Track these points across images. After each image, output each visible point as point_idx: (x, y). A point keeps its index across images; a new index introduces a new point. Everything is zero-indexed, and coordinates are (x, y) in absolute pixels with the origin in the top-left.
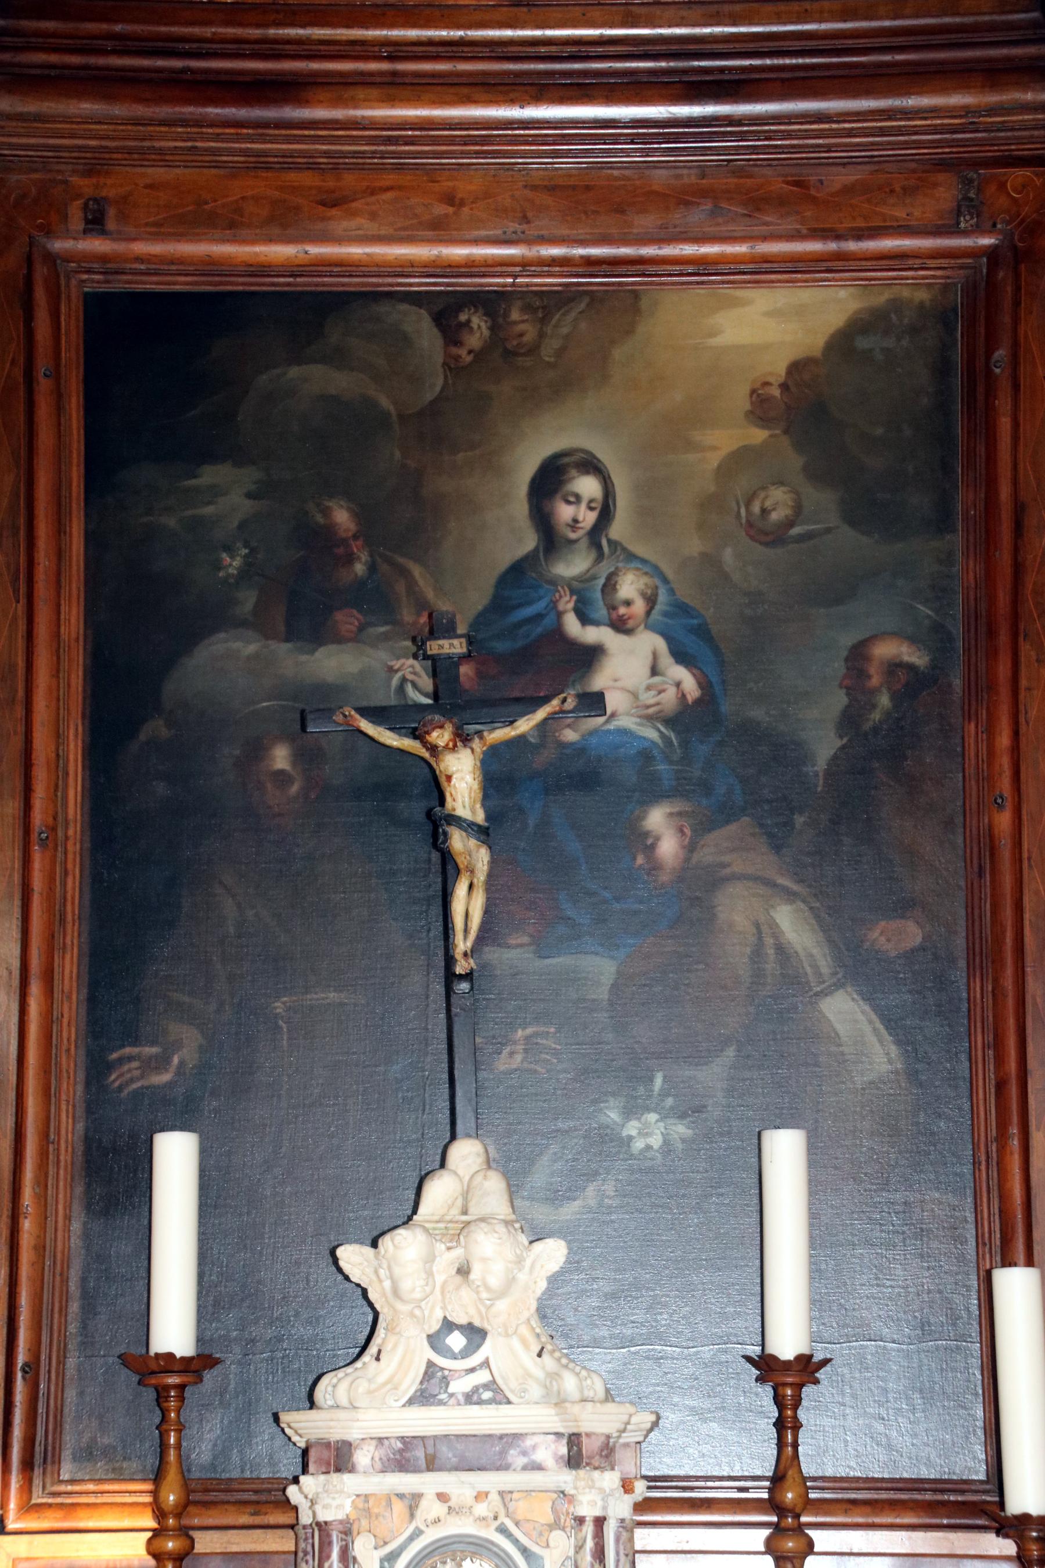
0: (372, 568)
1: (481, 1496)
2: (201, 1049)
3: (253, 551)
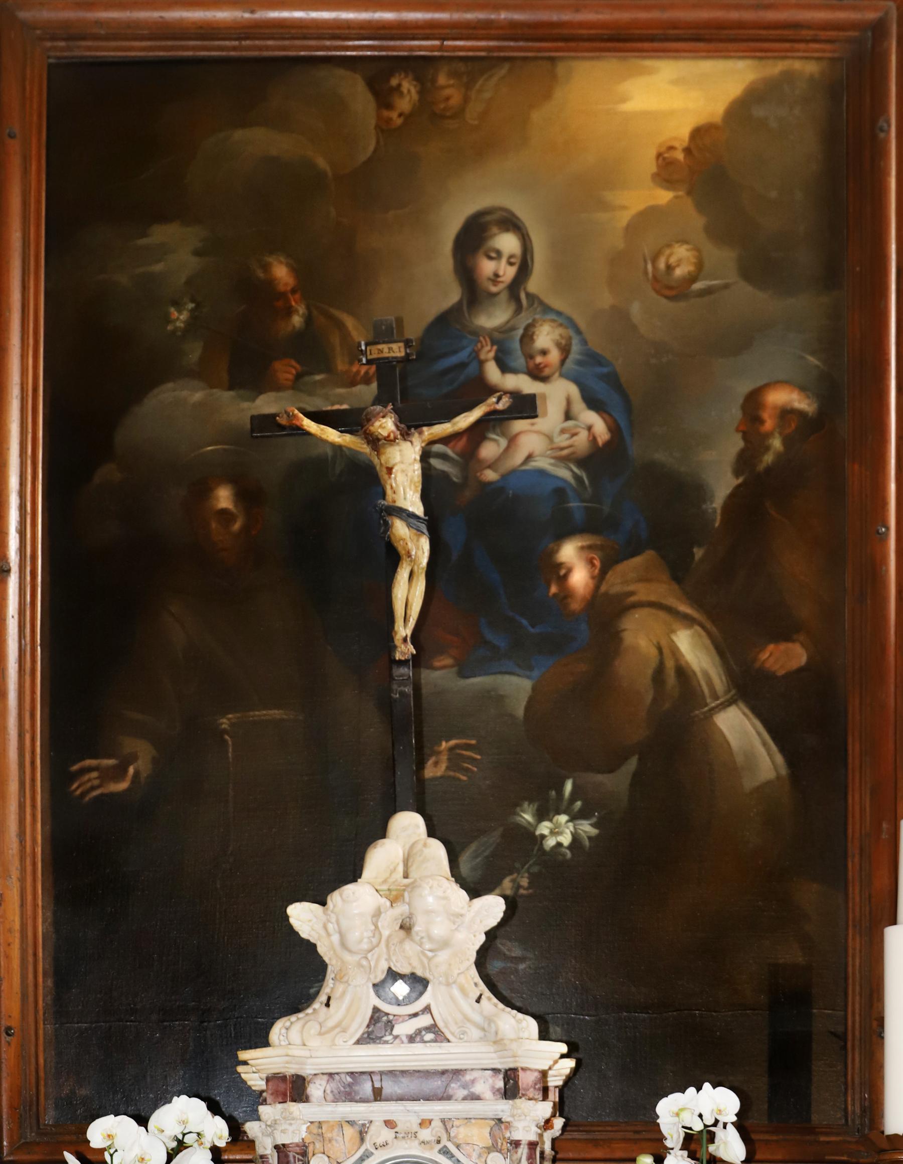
0: (309, 320)
1: (425, 1123)
2: (155, 761)
3: (198, 305)
